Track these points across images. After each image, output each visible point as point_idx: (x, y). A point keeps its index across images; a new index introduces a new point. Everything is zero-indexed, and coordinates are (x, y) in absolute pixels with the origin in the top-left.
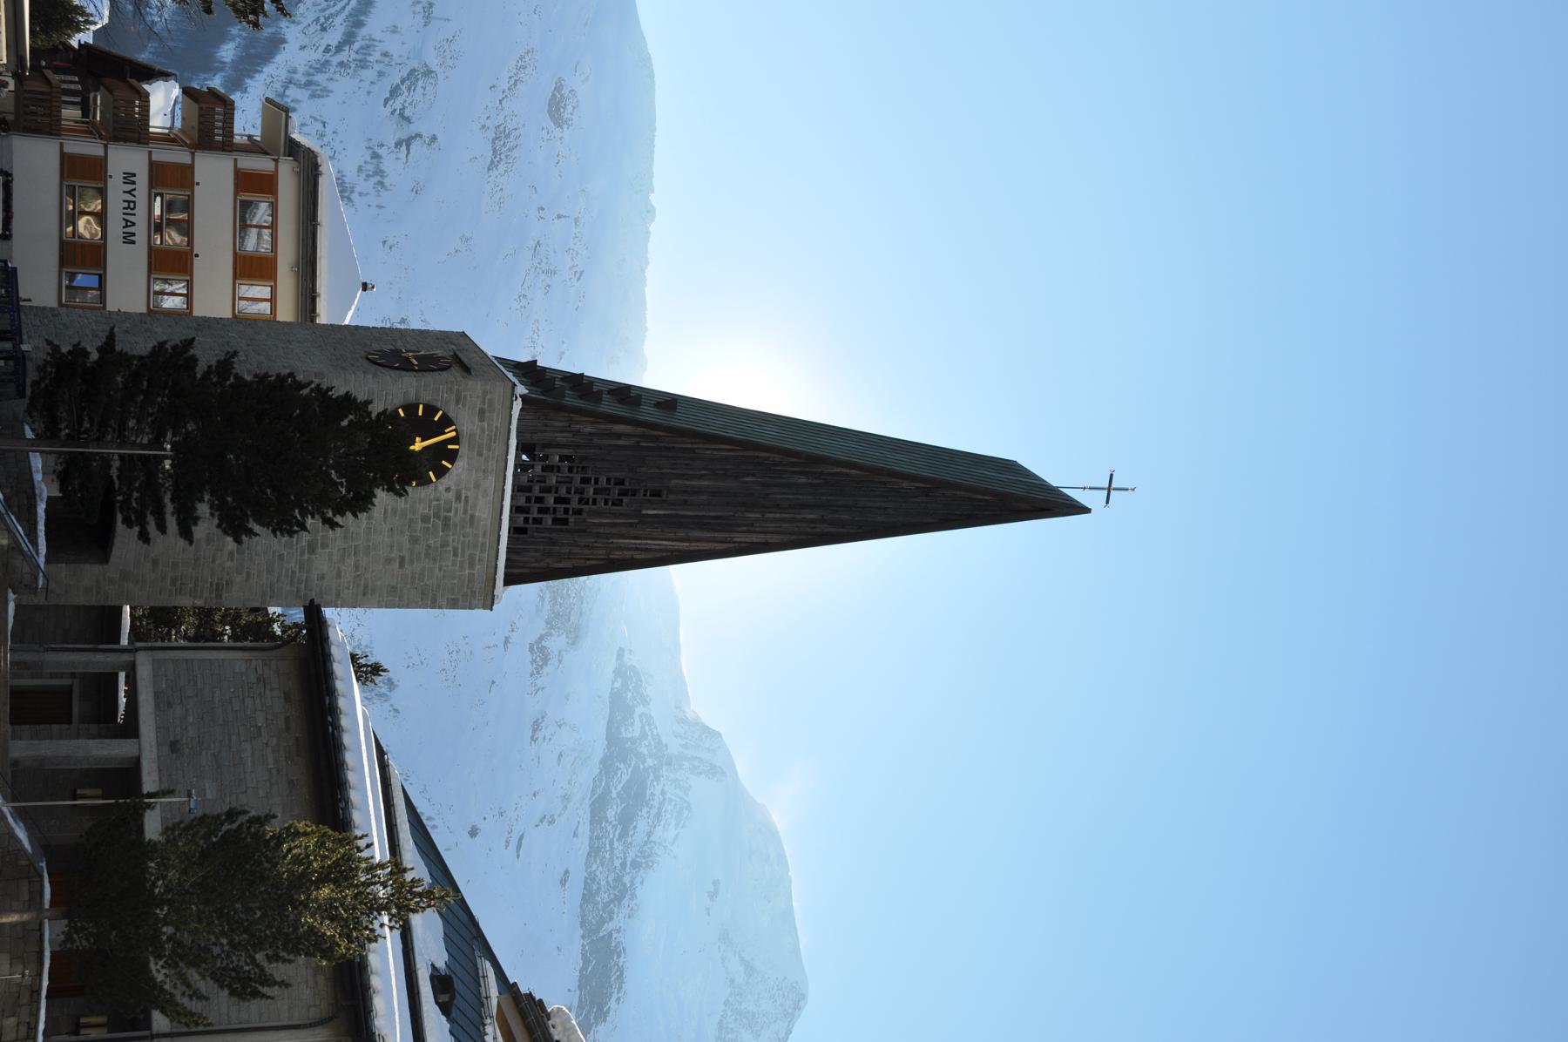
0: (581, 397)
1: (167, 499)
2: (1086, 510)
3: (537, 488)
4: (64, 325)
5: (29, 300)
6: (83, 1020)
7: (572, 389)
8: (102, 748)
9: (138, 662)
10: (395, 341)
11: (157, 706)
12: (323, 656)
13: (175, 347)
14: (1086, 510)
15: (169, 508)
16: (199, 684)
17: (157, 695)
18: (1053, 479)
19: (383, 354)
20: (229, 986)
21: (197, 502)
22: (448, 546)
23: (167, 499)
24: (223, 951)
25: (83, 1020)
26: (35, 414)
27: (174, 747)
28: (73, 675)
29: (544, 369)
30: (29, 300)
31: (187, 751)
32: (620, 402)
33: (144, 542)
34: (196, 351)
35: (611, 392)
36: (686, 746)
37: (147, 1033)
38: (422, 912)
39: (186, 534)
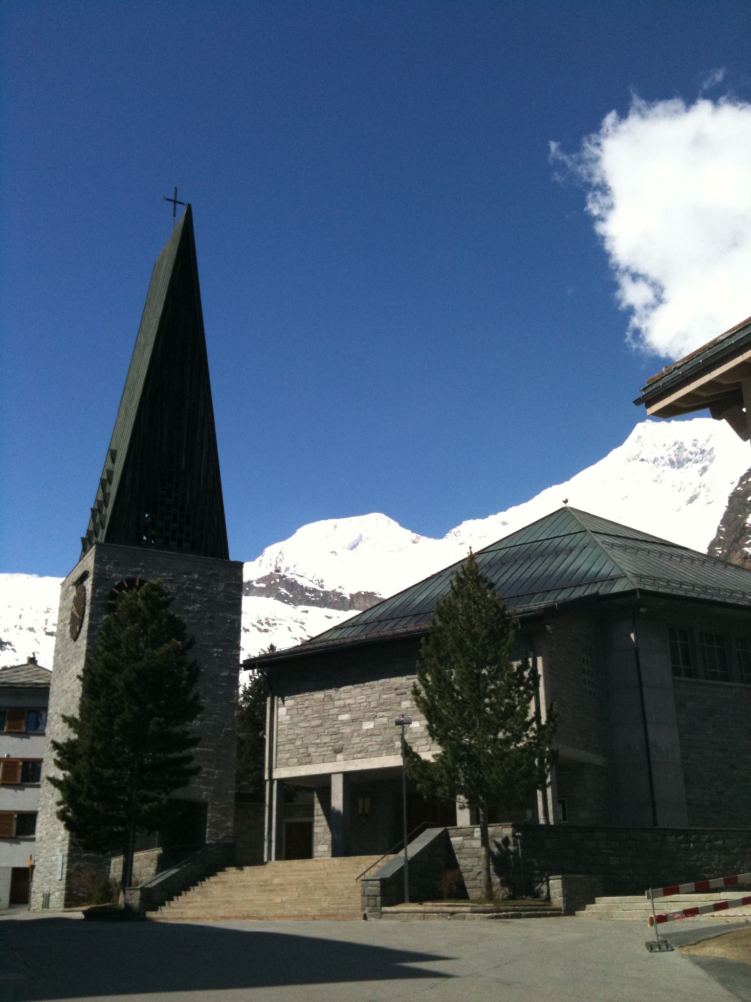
0: (107, 506)
1: (171, 756)
4: (47, 834)
5: (300, 626)
8: (337, 797)
10: (65, 625)
11: (310, 763)
13: (59, 754)
15: (177, 755)
16: (294, 737)
17: (300, 764)
19: (72, 630)
21: (620, 308)
22: (166, 252)
23: (171, 756)
26: (228, 650)
27: (338, 751)
30: (300, 626)
31: (340, 743)
34: (61, 740)
38: (678, 468)
39: (194, 742)
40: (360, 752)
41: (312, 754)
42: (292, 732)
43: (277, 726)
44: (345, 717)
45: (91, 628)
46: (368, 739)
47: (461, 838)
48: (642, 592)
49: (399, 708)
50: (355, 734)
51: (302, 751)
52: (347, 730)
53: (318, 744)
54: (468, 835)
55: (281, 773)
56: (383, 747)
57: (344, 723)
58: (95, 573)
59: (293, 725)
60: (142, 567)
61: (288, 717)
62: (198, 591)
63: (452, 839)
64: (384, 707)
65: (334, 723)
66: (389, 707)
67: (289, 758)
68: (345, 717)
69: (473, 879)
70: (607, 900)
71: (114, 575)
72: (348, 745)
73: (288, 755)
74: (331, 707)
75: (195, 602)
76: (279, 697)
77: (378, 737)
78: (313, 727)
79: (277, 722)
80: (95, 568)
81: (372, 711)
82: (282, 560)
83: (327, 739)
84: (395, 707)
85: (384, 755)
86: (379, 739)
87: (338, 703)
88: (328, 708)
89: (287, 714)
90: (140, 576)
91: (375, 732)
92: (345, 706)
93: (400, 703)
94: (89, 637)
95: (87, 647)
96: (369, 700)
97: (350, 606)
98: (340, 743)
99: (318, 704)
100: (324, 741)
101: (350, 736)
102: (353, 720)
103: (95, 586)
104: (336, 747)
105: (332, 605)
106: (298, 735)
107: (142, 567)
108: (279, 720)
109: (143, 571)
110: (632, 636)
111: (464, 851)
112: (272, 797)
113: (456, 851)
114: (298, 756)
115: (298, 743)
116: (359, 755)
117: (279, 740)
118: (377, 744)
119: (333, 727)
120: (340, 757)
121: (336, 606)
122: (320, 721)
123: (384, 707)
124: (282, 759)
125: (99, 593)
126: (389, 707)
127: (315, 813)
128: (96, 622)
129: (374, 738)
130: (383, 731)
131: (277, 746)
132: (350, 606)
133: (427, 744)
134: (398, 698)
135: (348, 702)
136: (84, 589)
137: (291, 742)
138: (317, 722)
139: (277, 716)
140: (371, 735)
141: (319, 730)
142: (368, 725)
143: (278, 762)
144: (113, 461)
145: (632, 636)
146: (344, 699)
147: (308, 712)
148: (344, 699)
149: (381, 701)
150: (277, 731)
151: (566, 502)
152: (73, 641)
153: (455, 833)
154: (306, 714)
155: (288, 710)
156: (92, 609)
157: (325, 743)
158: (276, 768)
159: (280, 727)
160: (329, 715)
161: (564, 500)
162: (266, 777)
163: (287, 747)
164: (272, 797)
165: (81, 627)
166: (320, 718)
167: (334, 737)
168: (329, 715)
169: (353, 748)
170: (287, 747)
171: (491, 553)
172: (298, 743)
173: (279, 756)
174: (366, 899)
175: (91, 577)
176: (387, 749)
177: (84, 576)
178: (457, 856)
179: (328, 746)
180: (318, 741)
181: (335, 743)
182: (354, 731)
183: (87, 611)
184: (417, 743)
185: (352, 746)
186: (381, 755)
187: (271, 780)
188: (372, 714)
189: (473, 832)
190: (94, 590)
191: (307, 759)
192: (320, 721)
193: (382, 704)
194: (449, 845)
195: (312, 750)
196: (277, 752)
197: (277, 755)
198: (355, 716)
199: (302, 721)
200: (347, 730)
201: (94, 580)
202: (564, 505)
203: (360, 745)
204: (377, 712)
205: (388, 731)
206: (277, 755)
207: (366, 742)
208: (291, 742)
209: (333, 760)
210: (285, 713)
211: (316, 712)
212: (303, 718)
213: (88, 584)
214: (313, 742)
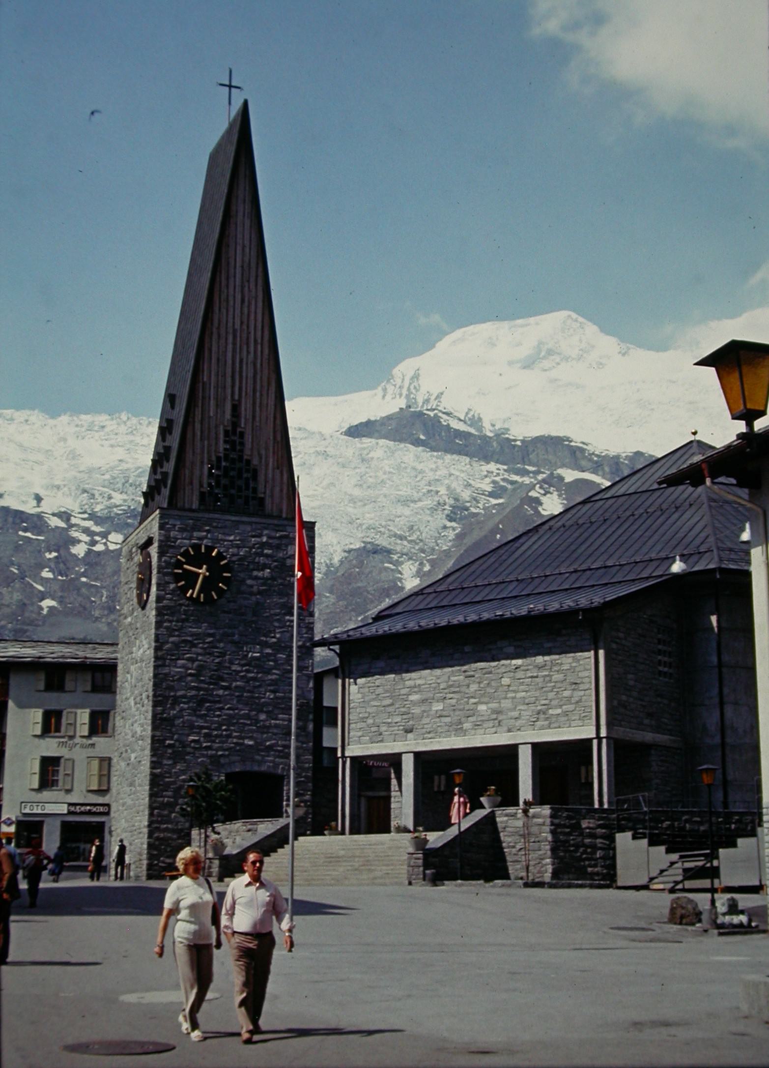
0: (168, 461)
2: (246, 104)
3: (233, 492)
6: (583, 781)
7: (162, 467)
9: (351, 755)
12: (378, 845)
14: (246, 104)
18: (224, 126)
19: (139, 596)
20: (241, 458)
24: (551, 700)
25: (583, 781)
28: (359, 796)
29: (149, 486)
31: (411, 723)
32: (170, 433)
33: (350, 428)
35: (164, 440)
36: (401, 395)
37: (595, 742)
40: (429, 733)
41: (384, 733)
42: (363, 710)
43: (349, 704)
44: (414, 697)
45: (159, 599)
46: (438, 720)
47: (505, 819)
48: (722, 571)
49: (467, 691)
50: (425, 714)
51: (373, 729)
52: (417, 710)
53: (389, 723)
54: (512, 816)
55: (354, 750)
56: (451, 729)
57: (414, 703)
58: (160, 541)
59: (365, 703)
60: (208, 531)
61: (360, 696)
62: (267, 556)
63: (498, 819)
64: (453, 689)
65: (405, 703)
66: (458, 689)
67: (360, 737)
68: (414, 697)
69: (515, 854)
70: (382, 844)
71: (179, 541)
72: (419, 725)
73: (360, 734)
74: (402, 687)
75: (264, 567)
76: (350, 678)
77: (447, 718)
78: (384, 706)
79: (349, 700)
80: (160, 534)
81: (441, 693)
82: (418, 388)
83: (398, 719)
84: (464, 689)
85: (453, 735)
86: (448, 720)
87: (408, 683)
88: (399, 687)
89: (358, 692)
90: (205, 541)
91: (444, 713)
92: (415, 687)
93: (468, 686)
94: (158, 609)
95: (156, 618)
96: (439, 681)
97: (523, 459)
98: (411, 723)
99: (389, 683)
100: (396, 721)
101: (421, 715)
102: (424, 701)
103: (161, 553)
104: (407, 727)
105: (496, 457)
106: (369, 713)
107: (208, 531)
108: (351, 698)
109: (209, 535)
110: (714, 619)
111: (507, 829)
112: (345, 776)
113: (500, 830)
114: (370, 734)
115: (370, 721)
116: (429, 736)
117: (351, 718)
118: (446, 725)
119: (404, 707)
120: (410, 736)
121: (501, 459)
122: (391, 701)
123: (453, 689)
124: (354, 736)
125: (165, 561)
126: (458, 689)
127: (392, 789)
128: (163, 593)
129: (443, 719)
130: (452, 713)
131: (349, 724)
132: (523, 459)
133: (493, 727)
134: (467, 681)
135: (419, 682)
136: (149, 555)
137: (364, 720)
138: (388, 702)
139: (349, 694)
140: (440, 716)
141: (391, 709)
142: (438, 707)
143: (351, 740)
144: (173, 407)
145: (714, 619)
146: (415, 679)
147: (380, 690)
148: (415, 679)
149: (451, 683)
150: (349, 709)
151: (695, 433)
152: (140, 609)
153: (501, 814)
154: (377, 693)
155: (359, 688)
156: (159, 579)
157: (396, 723)
158: (349, 745)
159: (352, 705)
160: (399, 695)
161: (693, 431)
162: (339, 754)
163: (359, 725)
164: (345, 776)
165: (148, 596)
166: (391, 697)
167: (405, 717)
168: (399, 695)
169: (423, 728)
170: (359, 725)
171: (598, 502)
172: (370, 721)
173: (351, 734)
174: (411, 869)
175: (156, 545)
176: (456, 730)
177: (149, 542)
178: (502, 834)
179: (399, 726)
180: (389, 720)
181: (406, 722)
182: (424, 711)
183: (154, 581)
184: (485, 726)
185: (422, 726)
186: (450, 736)
187: (343, 756)
188: (441, 695)
189: (516, 813)
190: (160, 558)
191: (379, 737)
192: (391, 701)
193: (451, 686)
194: (494, 823)
195: (383, 728)
196: (349, 729)
197: (349, 733)
198: (424, 697)
199: (374, 699)
200: (417, 710)
201: (160, 547)
202: (692, 438)
203: (430, 726)
204: (446, 694)
205: (457, 713)
206: (349, 733)
207: (435, 723)
208: (364, 720)
209: (404, 739)
210: (357, 691)
211: (386, 691)
212: (375, 697)
213: (154, 550)
214: (384, 721)
